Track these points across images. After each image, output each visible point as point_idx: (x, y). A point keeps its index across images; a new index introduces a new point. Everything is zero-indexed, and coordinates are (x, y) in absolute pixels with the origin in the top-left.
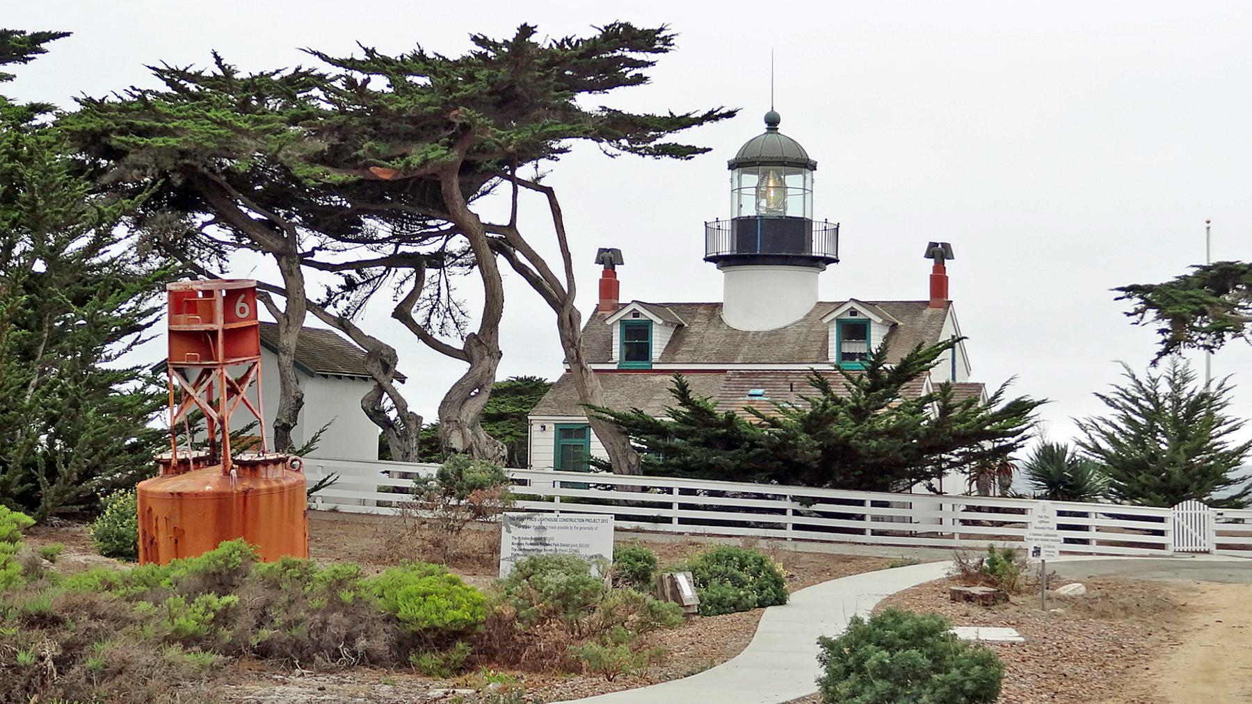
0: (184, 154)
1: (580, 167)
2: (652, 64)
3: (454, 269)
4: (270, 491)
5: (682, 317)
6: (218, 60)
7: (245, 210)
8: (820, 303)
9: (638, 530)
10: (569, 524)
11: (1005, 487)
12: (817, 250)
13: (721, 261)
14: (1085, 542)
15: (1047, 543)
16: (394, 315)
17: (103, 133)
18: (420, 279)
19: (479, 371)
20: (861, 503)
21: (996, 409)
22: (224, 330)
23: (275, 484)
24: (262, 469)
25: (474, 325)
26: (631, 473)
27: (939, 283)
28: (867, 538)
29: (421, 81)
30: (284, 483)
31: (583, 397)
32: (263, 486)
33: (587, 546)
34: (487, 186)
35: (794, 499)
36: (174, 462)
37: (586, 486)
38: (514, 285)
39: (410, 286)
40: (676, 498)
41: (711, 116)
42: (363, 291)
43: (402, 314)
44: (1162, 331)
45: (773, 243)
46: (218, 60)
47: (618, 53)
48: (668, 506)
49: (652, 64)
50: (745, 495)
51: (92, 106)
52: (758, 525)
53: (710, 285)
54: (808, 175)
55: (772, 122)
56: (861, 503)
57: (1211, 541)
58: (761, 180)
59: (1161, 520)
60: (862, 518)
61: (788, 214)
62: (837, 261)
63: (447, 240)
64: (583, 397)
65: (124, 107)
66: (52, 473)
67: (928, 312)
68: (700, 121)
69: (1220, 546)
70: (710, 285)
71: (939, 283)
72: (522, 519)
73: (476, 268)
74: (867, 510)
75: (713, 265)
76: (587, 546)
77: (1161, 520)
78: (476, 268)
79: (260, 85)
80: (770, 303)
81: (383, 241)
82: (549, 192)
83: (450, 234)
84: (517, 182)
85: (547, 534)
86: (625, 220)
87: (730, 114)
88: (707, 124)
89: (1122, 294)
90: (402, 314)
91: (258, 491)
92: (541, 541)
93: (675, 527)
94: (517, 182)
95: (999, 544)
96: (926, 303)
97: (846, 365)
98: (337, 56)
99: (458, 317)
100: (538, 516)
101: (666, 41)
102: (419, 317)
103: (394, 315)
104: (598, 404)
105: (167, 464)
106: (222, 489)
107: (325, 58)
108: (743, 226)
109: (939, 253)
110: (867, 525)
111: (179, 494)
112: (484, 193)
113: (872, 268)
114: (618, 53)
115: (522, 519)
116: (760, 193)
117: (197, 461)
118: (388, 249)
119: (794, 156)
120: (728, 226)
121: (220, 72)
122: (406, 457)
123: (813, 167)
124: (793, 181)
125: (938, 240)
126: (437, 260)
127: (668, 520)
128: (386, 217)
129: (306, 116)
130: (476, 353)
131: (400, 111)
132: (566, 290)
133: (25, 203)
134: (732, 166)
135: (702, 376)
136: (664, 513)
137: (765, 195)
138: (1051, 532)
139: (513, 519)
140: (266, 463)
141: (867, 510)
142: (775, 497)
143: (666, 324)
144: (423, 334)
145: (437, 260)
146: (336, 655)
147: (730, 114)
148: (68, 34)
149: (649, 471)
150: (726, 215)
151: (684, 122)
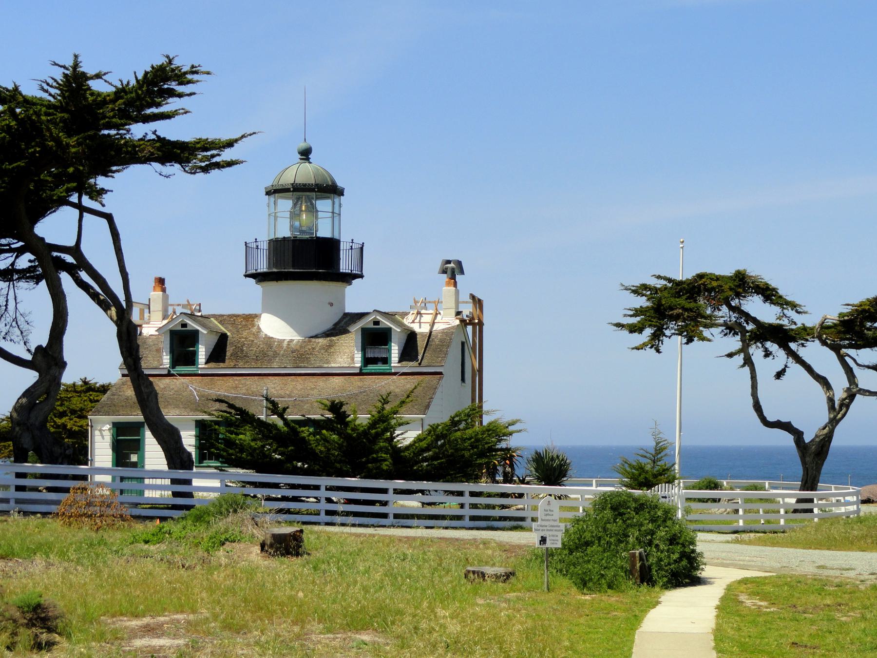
1: (128, 189)
8: (346, 315)
13: (260, 277)
15: (551, 533)
20: (384, 491)
25: (41, 337)
54: (337, 200)
55: (658, 351)
56: (384, 491)
58: (295, 205)
62: (361, 276)
63: (17, 257)
70: (248, 297)
73: (43, 283)
75: (252, 281)
78: (43, 283)
82: (109, 218)
83: (20, 252)
86: (173, 241)
94: (82, 209)
95: (259, 365)
108: (277, 246)
116: (294, 215)
120: (265, 246)
123: (339, 192)
124: (324, 205)
132: (124, 304)
135: (238, 378)
138: (555, 524)
141: (390, 497)
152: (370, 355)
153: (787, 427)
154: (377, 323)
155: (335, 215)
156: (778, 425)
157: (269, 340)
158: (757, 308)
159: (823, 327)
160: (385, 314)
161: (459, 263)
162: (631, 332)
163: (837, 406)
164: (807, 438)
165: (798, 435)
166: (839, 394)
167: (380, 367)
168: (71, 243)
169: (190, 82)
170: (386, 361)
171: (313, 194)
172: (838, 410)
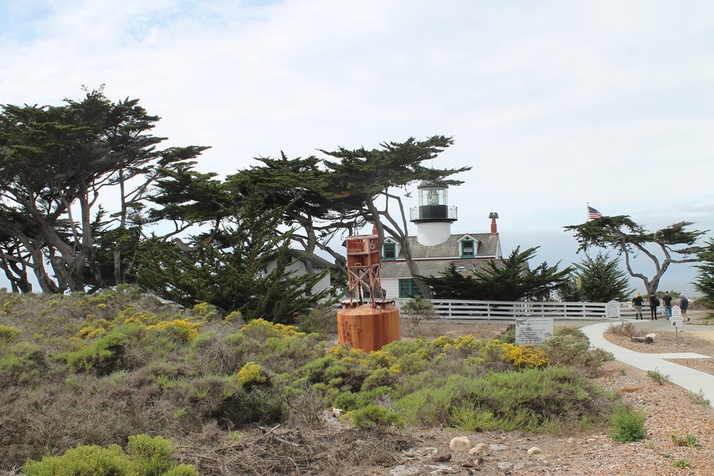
2: (443, 151)
4: (391, 313)
7: (180, 205)
11: (547, 297)
14: (581, 316)
17: (247, 182)
22: (371, 254)
27: (494, 227)
28: (489, 317)
29: (364, 159)
35: (490, 305)
41: (462, 170)
44: (580, 242)
46: (283, 153)
47: (431, 147)
48: (448, 309)
49: (443, 151)
52: (474, 315)
57: (619, 313)
59: (604, 307)
61: (440, 204)
68: (457, 172)
69: (622, 315)
71: (494, 227)
72: (522, 321)
74: (450, 307)
77: (604, 307)
79: (297, 163)
81: (338, 218)
84: (388, 195)
85: (531, 326)
87: (469, 169)
88: (460, 173)
89: (567, 229)
91: (388, 314)
92: (529, 329)
93: (450, 317)
94: (388, 195)
98: (330, 152)
101: (451, 143)
109: (494, 216)
110: (450, 312)
111: (360, 316)
113: (469, 217)
116: (429, 196)
120: (418, 209)
124: (440, 192)
126: (355, 224)
127: (448, 314)
136: (447, 312)
142: (480, 305)
147: (469, 169)
148: (210, 147)
149: (436, 297)
151: (452, 172)
152: (465, 251)
153: (640, 276)
154: (468, 238)
155: (445, 196)
156: (640, 276)
157: (422, 247)
158: (625, 230)
159: (659, 234)
160: (471, 235)
161: (496, 214)
162: (190, 148)
163: (661, 267)
164: (649, 281)
165: (645, 279)
166: (661, 263)
167: (469, 256)
168: (384, 210)
169: (149, 127)
170: (471, 254)
172: (662, 270)
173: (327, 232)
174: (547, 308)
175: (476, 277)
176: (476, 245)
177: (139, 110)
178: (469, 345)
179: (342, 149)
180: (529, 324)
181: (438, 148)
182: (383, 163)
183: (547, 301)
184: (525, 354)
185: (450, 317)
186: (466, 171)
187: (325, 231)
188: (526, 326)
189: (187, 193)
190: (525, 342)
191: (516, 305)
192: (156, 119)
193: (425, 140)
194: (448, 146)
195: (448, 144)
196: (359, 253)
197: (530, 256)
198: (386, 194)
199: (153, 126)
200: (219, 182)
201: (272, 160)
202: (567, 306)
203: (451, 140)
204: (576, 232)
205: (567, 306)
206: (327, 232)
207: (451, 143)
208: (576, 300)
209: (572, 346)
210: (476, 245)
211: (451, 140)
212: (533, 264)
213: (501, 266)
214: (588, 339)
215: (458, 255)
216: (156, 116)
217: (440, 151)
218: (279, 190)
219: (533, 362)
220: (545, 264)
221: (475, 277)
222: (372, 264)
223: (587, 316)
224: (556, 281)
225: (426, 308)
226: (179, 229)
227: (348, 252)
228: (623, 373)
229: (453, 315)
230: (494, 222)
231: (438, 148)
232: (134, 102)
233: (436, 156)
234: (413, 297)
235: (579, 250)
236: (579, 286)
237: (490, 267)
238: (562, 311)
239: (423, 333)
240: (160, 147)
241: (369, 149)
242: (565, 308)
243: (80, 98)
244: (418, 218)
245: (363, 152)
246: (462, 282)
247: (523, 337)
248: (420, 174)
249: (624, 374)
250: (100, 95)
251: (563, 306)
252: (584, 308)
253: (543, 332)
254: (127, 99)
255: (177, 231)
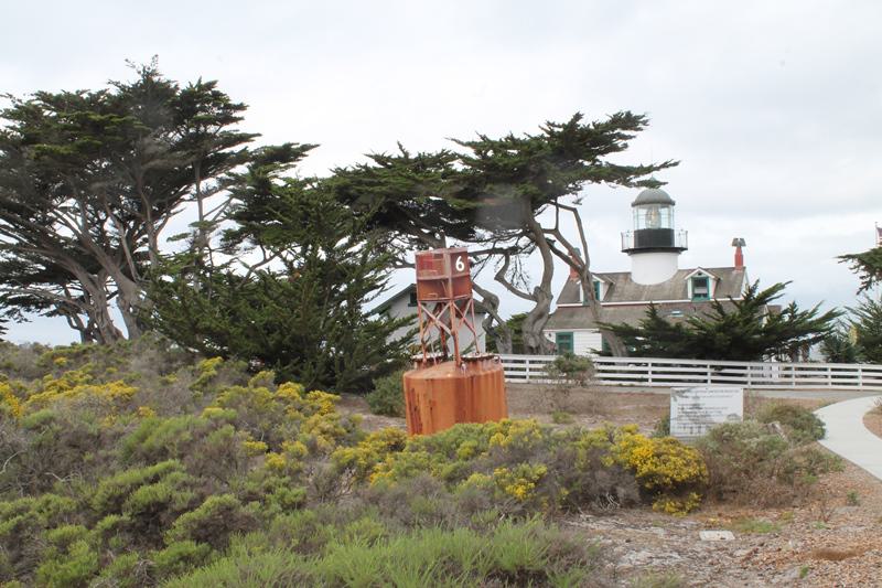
0: (388, 196)
3: (522, 255)
4: (486, 376)
5: (612, 280)
6: (401, 147)
8: (679, 271)
9: (632, 386)
10: (714, 394)
11: (805, 357)
12: (677, 245)
13: (631, 252)
14: (856, 384)
16: (496, 279)
17: (348, 186)
18: (507, 260)
19: (542, 306)
21: (814, 318)
22: (453, 279)
23: (489, 372)
24: (480, 363)
26: (623, 356)
27: (739, 258)
30: (494, 371)
31: (597, 318)
32: (482, 373)
33: (726, 408)
34: (540, 209)
35: (712, 367)
36: (424, 360)
37: (613, 364)
38: (556, 259)
39: (503, 263)
40: (650, 368)
41: (665, 165)
42: (477, 268)
43: (499, 278)
44: (862, 278)
45: (656, 241)
46: (401, 147)
50: (683, 366)
51: (341, 173)
53: (625, 264)
60: (524, 370)
62: (686, 249)
64: (597, 318)
65: (356, 173)
66: (342, 367)
67: (734, 272)
68: (658, 169)
71: (739, 258)
72: (683, 392)
76: (726, 408)
79: (423, 162)
80: (652, 271)
81: (488, 240)
83: (520, 236)
84: (558, 206)
85: (700, 402)
87: (676, 164)
88: (662, 170)
90: (499, 278)
91: (479, 377)
92: (696, 406)
94: (558, 206)
96: (733, 269)
97: (697, 300)
99: (526, 278)
100: (694, 390)
101: (645, 123)
102: (508, 279)
103: (496, 279)
104: (604, 322)
105: (420, 362)
106: (456, 376)
107: (459, 143)
109: (739, 244)
110: (860, 380)
111: (432, 380)
112: (539, 213)
113: (704, 249)
114: (616, 132)
115: (683, 392)
116: (648, 217)
117: (438, 359)
118: (490, 246)
119: (665, 198)
120: (632, 235)
121: (402, 155)
122: (506, 352)
123: (673, 203)
124: (664, 211)
125: (739, 237)
126: (514, 250)
127: (647, 380)
128: (487, 228)
129: (451, 173)
130: (540, 298)
131: (506, 165)
133: (314, 218)
134: (633, 205)
136: (645, 376)
137: (650, 219)
139: (678, 392)
140: (482, 359)
142: (698, 366)
143: (606, 283)
144: (511, 287)
145: (514, 250)
146: (604, 499)
147: (676, 164)
150: (633, 229)
151: (650, 169)
162: (287, 147)
168: (553, 227)
169: (236, 120)
170: (706, 295)
171: (659, 205)
173: (475, 261)
174: (533, 366)
175: (690, 326)
176: (711, 284)
177: (217, 95)
178: (526, 439)
179: (483, 138)
180: (697, 398)
181: (626, 133)
182: (539, 154)
183: (806, 361)
184: (659, 456)
185: (650, 383)
186: (671, 168)
187: (472, 259)
188: (690, 401)
189: (267, 209)
190: (688, 430)
191: (752, 368)
192: (241, 107)
193: (604, 119)
194: (640, 129)
195: (640, 126)
196: (434, 278)
197: (776, 295)
198: (555, 204)
199: (241, 119)
200: (779, 307)
201: (389, 157)
202: (833, 370)
203: (644, 119)
204: (856, 262)
205: (833, 370)
206: (475, 261)
207: (645, 123)
208: (849, 360)
209: (753, 443)
210: (711, 284)
211: (644, 119)
212: (781, 302)
213: (731, 310)
214: (824, 424)
215: (687, 298)
216: (242, 104)
217: (630, 137)
218: (396, 197)
219: (670, 473)
220: (793, 306)
221: (687, 326)
222: (455, 295)
223: (864, 384)
224: (812, 331)
225: (578, 369)
226: (268, 257)
227: (418, 274)
228: (852, 500)
229: (654, 380)
230: (739, 251)
231: (626, 133)
232: (210, 85)
233: (626, 146)
234: (561, 353)
235: (861, 289)
236: (853, 339)
237: (715, 311)
238: (826, 376)
239: (571, 408)
240: (251, 147)
241: (520, 135)
242: (830, 373)
243: (132, 78)
244: (632, 247)
245: (513, 142)
246: (669, 333)
247: (685, 420)
248: (620, 175)
249: (855, 503)
250: (154, 73)
251: (825, 370)
252: (860, 373)
253: (724, 412)
254: (200, 81)
255: (265, 261)
